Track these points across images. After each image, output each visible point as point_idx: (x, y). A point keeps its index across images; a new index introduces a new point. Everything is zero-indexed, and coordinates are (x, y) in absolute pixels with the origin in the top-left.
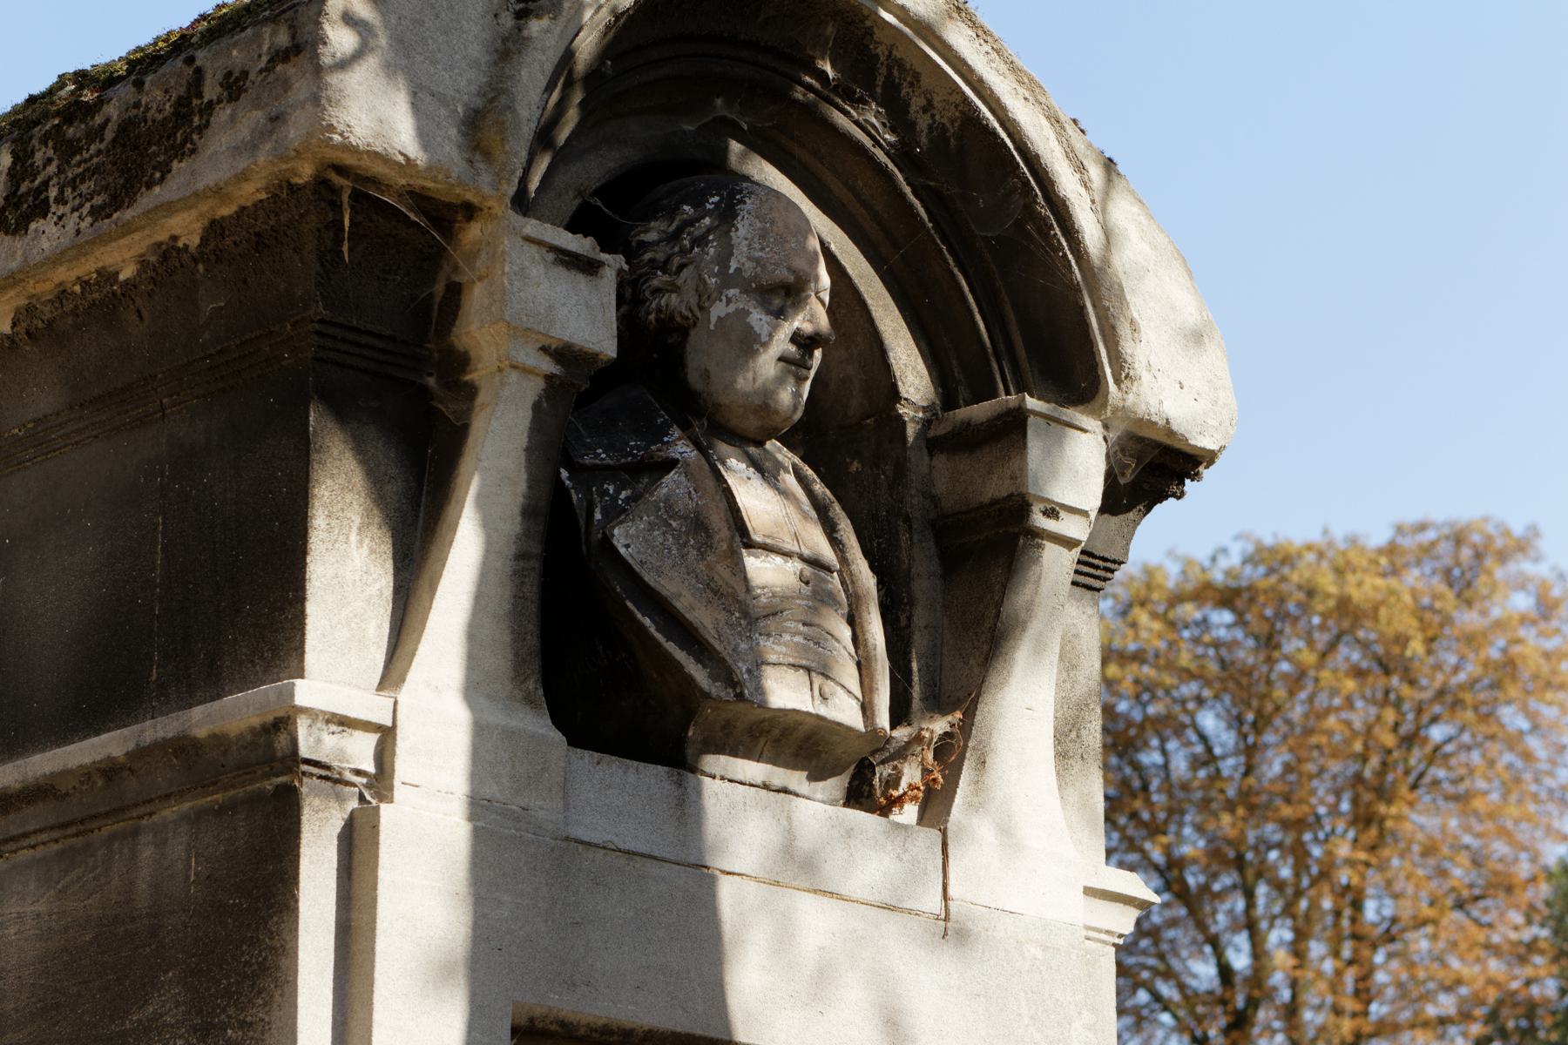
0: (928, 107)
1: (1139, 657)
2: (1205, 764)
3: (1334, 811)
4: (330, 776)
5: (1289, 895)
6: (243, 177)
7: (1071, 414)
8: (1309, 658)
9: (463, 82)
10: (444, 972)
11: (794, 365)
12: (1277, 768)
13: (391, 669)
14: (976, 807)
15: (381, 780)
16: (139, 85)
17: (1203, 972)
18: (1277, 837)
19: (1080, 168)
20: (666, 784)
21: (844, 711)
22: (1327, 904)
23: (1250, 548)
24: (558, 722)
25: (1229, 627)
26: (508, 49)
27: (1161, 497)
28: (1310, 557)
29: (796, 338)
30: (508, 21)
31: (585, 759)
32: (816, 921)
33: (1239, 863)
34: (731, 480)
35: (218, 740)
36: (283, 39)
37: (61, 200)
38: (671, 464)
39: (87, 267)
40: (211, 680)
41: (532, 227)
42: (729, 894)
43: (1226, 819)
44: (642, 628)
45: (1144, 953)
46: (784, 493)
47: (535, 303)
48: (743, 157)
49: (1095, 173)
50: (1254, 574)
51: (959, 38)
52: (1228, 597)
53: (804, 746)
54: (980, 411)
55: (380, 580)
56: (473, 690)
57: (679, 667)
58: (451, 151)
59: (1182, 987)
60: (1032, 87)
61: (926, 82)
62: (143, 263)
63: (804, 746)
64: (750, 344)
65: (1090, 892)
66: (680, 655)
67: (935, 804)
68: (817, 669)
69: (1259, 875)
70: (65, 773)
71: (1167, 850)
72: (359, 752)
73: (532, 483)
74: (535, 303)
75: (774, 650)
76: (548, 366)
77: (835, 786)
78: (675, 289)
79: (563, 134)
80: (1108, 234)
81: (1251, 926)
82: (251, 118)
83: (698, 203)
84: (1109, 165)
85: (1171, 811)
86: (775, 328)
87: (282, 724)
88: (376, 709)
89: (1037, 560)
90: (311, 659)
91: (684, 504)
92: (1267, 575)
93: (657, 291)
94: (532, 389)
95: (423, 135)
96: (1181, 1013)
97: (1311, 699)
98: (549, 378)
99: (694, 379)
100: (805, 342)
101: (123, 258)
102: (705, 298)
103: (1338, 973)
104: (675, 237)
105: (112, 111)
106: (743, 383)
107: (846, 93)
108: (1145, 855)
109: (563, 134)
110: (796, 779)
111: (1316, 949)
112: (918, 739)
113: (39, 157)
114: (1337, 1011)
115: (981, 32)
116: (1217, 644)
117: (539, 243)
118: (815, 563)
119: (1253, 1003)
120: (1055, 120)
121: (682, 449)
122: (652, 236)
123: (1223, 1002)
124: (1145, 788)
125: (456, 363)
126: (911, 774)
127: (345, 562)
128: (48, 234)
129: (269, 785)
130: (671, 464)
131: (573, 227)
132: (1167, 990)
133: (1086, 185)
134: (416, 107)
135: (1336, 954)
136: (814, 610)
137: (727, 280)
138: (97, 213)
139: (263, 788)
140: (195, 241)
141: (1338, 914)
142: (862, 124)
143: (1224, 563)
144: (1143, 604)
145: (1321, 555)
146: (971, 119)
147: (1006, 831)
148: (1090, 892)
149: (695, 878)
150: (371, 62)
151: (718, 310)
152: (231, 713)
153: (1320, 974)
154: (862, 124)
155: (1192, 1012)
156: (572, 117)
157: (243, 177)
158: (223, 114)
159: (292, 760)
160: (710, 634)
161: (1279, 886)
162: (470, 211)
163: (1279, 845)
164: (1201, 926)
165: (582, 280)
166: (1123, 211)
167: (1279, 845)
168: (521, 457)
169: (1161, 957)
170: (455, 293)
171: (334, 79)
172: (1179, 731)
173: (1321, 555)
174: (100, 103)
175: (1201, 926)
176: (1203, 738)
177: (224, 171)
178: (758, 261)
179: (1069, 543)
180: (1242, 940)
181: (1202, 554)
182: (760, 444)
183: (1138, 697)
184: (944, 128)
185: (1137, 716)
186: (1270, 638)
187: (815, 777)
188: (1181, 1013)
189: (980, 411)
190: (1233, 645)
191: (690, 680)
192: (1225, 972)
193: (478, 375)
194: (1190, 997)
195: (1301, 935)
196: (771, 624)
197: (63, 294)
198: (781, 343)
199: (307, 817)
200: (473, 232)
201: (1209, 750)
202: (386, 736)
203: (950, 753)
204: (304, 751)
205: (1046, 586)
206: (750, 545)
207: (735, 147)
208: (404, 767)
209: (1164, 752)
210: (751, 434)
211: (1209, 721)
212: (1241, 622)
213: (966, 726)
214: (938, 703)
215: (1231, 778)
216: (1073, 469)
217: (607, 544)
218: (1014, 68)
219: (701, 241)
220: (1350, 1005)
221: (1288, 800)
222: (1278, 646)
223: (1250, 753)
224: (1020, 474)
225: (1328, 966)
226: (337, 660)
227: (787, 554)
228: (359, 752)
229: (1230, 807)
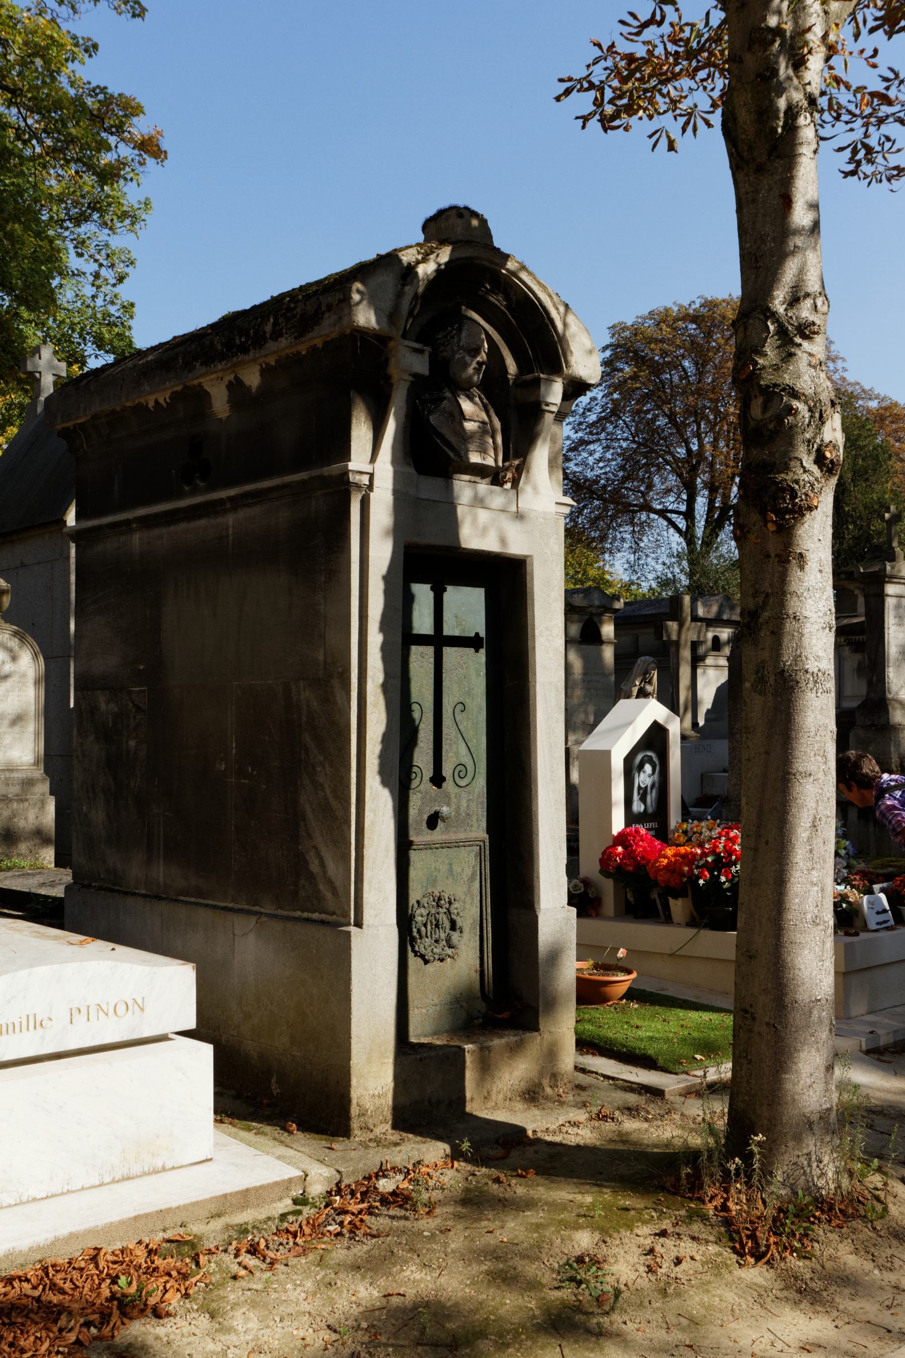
1: (662, 341)
2: (684, 378)
3: (729, 396)
4: (358, 486)
5: (712, 425)
6: (332, 332)
7: (552, 377)
8: (722, 341)
9: (388, 305)
10: (387, 533)
11: (477, 370)
12: (710, 380)
13: (372, 459)
14: (525, 483)
15: (370, 487)
16: (305, 304)
17: (681, 452)
18: (709, 405)
19: (557, 309)
21: (490, 462)
22: (726, 428)
23: (703, 301)
24: (416, 470)
25: (695, 329)
26: (399, 295)
28: (724, 304)
29: (478, 363)
30: (400, 287)
31: (422, 478)
32: (483, 516)
33: (696, 414)
34: (461, 401)
35: (330, 476)
36: (341, 296)
37: (286, 333)
38: (445, 398)
39: (294, 350)
40: (328, 460)
41: (407, 343)
42: (460, 510)
43: (691, 398)
45: (662, 446)
46: (475, 404)
47: (408, 362)
48: (465, 310)
49: (562, 309)
50: (704, 311)
51: (524, 276)
52: (695, 318)
53: (480, 471)
54: (529, 377)
55: (370, 435)
56: (394, 462)
57: (446, 453)
58: (385, 325)
59: (674, 456)
60: (544, 288)
62: (308, 352)
63: (480, 471)
64: (466, 365)
65: (557, 503)
66: (447, 449)
67: (515, 483)
68: (483, 451)
69: (702, 418)
70: (292, 482)
71: (670, 409)
72: (365, 480)
73: (408, 408)
74: (408, 362)
75: (472, 447)
76: (411, 378)
77: (488, 480)
78: (445, 351)
79: (416, 312)
80: (565, 325)
81: (698, 435)
82: (334, 317)
84: (567, 306)
85: (672, 396)
86: (472, 361)
87: (346, 472)
88: (368, 468)
89: (543, 417)
90: (352, 457)
92: (709, 311)
93: (441, 352)
94: (407, 385)
95: (378, 321)
96: (674, 466)
97: (722, 356)
100: (480, 364)
101: (303, 349)
103: (728, 453)
105: (298, 310)
106: (464, 376)
107: (492, 291)
108: (664, 412)
109: (416, 312)
110: (478, 479)
111: (722, 444)
112: (511, 466)
113: (280, 321)
114: (727, 466)
115: (530, 273)
116: (690, 336)
118: (483, 423)
119: (698, 463)
120: (550, 296)
121: (448, 394)
123: (688, 462)
124: (664, 387)
125: (388, 378)
126: (509, 475)
127: (361, 432)
128: (283, 342)
129: (343, 488)
130: (445, 398)
131: (416, 341)
132: (668, 457)
133: (559, 314)
134: (376, 314)
135: (728, 446)
136: (482, 436)
137: (460, 348)
138: (296, 338)
139: (341, 489)
140: (321, 346)
141: (729, 432)
142: (497, 300)
143: (693, 307)
144: (664, 322)
145: (728, 303)
147: (535, 488)
148: (557, 503)
149: (450, 506)
150: (365, 302)
151: (457, 356)
152: (334, 469)
153: (722, 453)
154: (497, 300)
155: (678, 465)
156: (418, 306)
157: (332, 332)
158: (327, 315)
159: (348, 482)
160: (454, 444)
161: (708, 421)
162: (391, 339)
163: (708, 408)
164: (682, 436)
165: (420, 356)
166: (571, 319)
167: (708, 408)
169: (667, 447)
170: (387, 361)
171: (354, 308)
172: (676, 368)
173: (728, 303)
174: (295, 307)
175: (682, 436)
176: (684, 370)
177: (326, 330)
179: (552, 412)
180: (695, 440)
181: (686, 303)
182: (469, 390)
183: (661, 355)
185: (661, 361)
186: (709, 334)
187: (483, 478)
188: (674, 466)
189: (529, 377)
190: (696, 336)
192: (689, 450)
193: (394, 381)
194: (676, 460)
195: (716, 440)
196: (470, 440)
197: (288, 356)
198: (474, 365)
199: (352, 496)
200: (392, 344)
201: (686, 373)
202: (372, 476)
203: (519, 470)
204: (351, 480)
205: (546, 424)
206: (465, 420)
207: (464, 307)
208: (376, 483)
209: (670, 375)
210: (466, 389)
211: (686, 364)
212: (699, 327)
213: (524, 462)
214: (517, 456)
215: (693, 384)
216: (555, 393)
217: (428, 420)
218: (539, 283)
219: (453, 337)
220: (731, 463)
221: (713, 393)
222: (711, 337)
223: (700, 374)
224: (538, 395)
225: (725, 450)
226: (358, 460)
227: (475, 421)
228: (365, 480)
229: (692, 394)
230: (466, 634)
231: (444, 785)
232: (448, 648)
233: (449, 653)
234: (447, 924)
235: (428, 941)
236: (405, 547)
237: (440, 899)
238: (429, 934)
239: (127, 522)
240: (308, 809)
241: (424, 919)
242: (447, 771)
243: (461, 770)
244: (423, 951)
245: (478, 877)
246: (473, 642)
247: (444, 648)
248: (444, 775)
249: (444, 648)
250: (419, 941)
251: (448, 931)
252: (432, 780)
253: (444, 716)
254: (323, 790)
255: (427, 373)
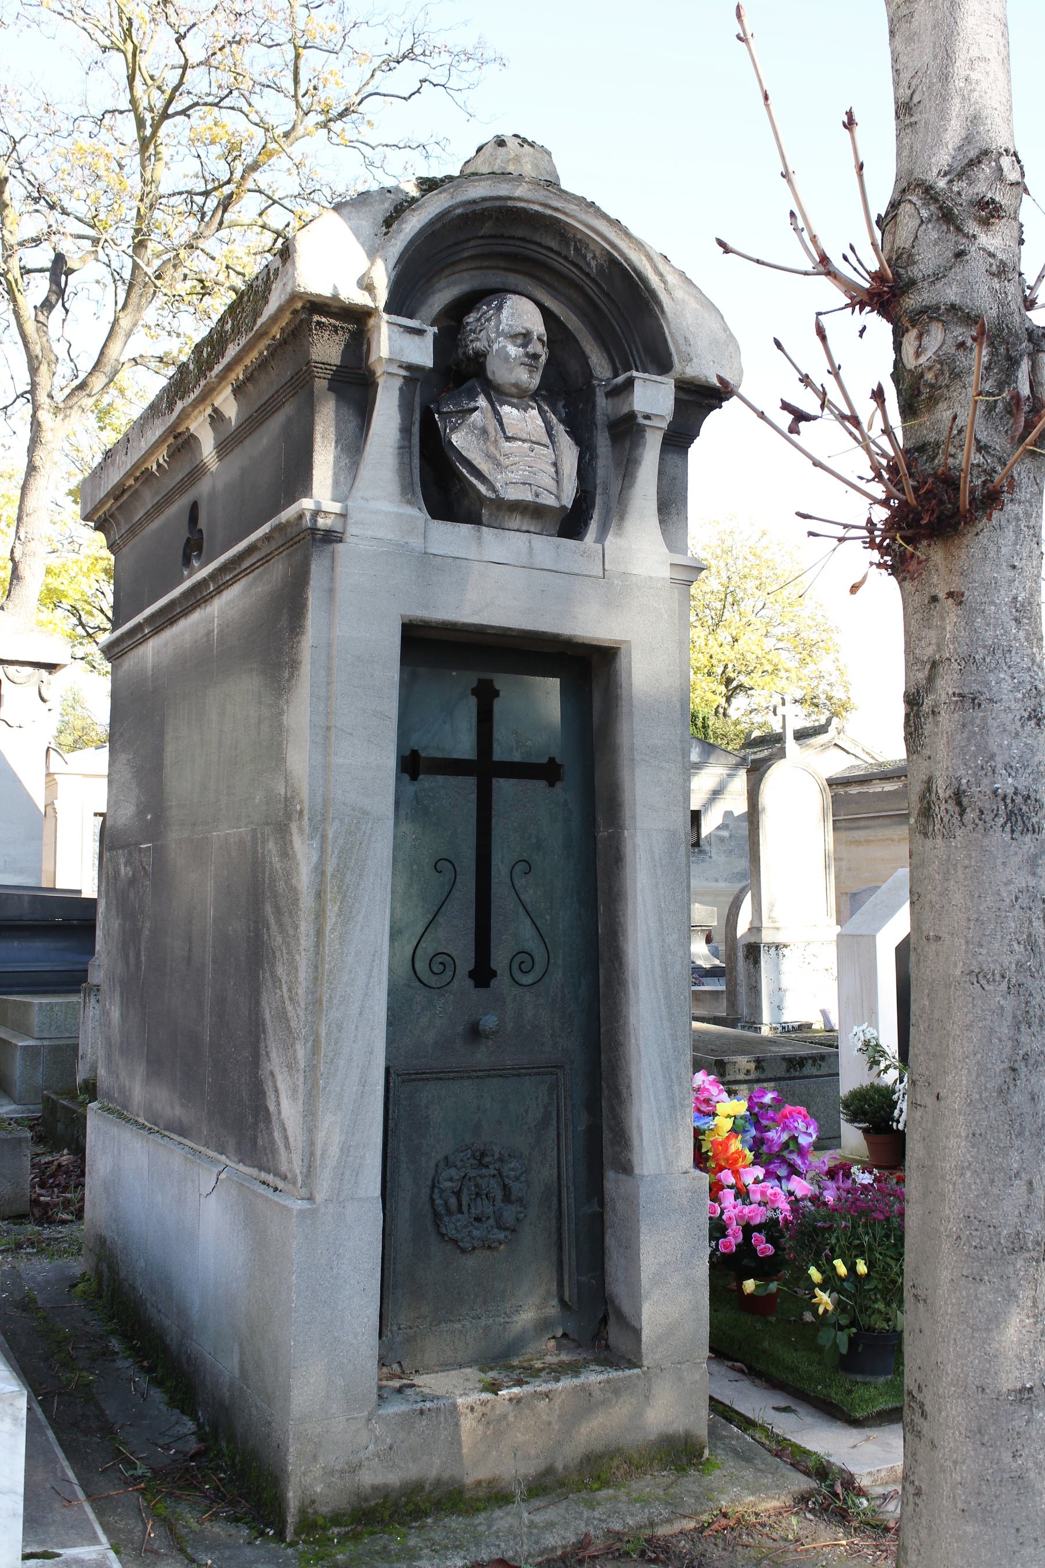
0: (594, 257)
20: (472, 532)
27: (712, 408)
44: (462, 473)
61: (592, 247)
66: (472, 479)
74: (398, 347)
76: (403, 373)
78: (478, 339)
83: (489, 305)
91: (480, 424)
93: (472, 341)
94: (398, 382)
98: (404, 377)
99: (490, 375)
102: (490, 342)
104: (479, 319)
117: (400, 325)
121: (482, 402)
122: (471, 320)
130: (476, 409)
137: (499, 334)
146: (613, 261)
151: (495, 347)
160: (486, 473)
165: (416, 338)
168: (397, 409)
178: (510, 326)
184: (602, 265)
191: (478, 492)
219: (489, 320)
227: (524, 441)
230: (534, 760)
231: (494, 983)
232: (501, 780)
233: (504, 788)
234: (499, 1194)
235: (462, 1219)
236: (404, 626)
237: (483, 1155)
238: (465, 1208)
239: (139, 627)
240: (267, 1016)
241: (456, 1185)
242: (499, 959)
243: (523, 960)
244: (452, 1233)
245: (554, 1122)
246: (547, 772)
247: (494, 780)
248: (493, 966)
249: (494, 780)
250: (446, 1219)
251: (499, 1203)
252: (472, 974)
253: (495, 880)
254: (281, 988)
255: (430, 363)
